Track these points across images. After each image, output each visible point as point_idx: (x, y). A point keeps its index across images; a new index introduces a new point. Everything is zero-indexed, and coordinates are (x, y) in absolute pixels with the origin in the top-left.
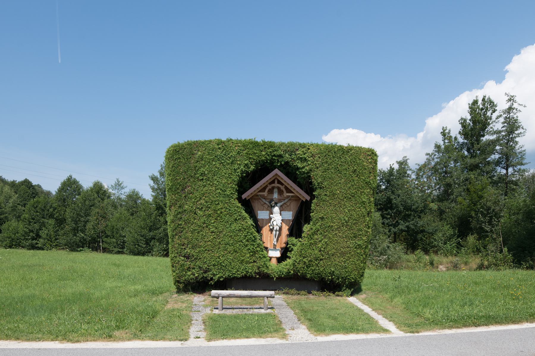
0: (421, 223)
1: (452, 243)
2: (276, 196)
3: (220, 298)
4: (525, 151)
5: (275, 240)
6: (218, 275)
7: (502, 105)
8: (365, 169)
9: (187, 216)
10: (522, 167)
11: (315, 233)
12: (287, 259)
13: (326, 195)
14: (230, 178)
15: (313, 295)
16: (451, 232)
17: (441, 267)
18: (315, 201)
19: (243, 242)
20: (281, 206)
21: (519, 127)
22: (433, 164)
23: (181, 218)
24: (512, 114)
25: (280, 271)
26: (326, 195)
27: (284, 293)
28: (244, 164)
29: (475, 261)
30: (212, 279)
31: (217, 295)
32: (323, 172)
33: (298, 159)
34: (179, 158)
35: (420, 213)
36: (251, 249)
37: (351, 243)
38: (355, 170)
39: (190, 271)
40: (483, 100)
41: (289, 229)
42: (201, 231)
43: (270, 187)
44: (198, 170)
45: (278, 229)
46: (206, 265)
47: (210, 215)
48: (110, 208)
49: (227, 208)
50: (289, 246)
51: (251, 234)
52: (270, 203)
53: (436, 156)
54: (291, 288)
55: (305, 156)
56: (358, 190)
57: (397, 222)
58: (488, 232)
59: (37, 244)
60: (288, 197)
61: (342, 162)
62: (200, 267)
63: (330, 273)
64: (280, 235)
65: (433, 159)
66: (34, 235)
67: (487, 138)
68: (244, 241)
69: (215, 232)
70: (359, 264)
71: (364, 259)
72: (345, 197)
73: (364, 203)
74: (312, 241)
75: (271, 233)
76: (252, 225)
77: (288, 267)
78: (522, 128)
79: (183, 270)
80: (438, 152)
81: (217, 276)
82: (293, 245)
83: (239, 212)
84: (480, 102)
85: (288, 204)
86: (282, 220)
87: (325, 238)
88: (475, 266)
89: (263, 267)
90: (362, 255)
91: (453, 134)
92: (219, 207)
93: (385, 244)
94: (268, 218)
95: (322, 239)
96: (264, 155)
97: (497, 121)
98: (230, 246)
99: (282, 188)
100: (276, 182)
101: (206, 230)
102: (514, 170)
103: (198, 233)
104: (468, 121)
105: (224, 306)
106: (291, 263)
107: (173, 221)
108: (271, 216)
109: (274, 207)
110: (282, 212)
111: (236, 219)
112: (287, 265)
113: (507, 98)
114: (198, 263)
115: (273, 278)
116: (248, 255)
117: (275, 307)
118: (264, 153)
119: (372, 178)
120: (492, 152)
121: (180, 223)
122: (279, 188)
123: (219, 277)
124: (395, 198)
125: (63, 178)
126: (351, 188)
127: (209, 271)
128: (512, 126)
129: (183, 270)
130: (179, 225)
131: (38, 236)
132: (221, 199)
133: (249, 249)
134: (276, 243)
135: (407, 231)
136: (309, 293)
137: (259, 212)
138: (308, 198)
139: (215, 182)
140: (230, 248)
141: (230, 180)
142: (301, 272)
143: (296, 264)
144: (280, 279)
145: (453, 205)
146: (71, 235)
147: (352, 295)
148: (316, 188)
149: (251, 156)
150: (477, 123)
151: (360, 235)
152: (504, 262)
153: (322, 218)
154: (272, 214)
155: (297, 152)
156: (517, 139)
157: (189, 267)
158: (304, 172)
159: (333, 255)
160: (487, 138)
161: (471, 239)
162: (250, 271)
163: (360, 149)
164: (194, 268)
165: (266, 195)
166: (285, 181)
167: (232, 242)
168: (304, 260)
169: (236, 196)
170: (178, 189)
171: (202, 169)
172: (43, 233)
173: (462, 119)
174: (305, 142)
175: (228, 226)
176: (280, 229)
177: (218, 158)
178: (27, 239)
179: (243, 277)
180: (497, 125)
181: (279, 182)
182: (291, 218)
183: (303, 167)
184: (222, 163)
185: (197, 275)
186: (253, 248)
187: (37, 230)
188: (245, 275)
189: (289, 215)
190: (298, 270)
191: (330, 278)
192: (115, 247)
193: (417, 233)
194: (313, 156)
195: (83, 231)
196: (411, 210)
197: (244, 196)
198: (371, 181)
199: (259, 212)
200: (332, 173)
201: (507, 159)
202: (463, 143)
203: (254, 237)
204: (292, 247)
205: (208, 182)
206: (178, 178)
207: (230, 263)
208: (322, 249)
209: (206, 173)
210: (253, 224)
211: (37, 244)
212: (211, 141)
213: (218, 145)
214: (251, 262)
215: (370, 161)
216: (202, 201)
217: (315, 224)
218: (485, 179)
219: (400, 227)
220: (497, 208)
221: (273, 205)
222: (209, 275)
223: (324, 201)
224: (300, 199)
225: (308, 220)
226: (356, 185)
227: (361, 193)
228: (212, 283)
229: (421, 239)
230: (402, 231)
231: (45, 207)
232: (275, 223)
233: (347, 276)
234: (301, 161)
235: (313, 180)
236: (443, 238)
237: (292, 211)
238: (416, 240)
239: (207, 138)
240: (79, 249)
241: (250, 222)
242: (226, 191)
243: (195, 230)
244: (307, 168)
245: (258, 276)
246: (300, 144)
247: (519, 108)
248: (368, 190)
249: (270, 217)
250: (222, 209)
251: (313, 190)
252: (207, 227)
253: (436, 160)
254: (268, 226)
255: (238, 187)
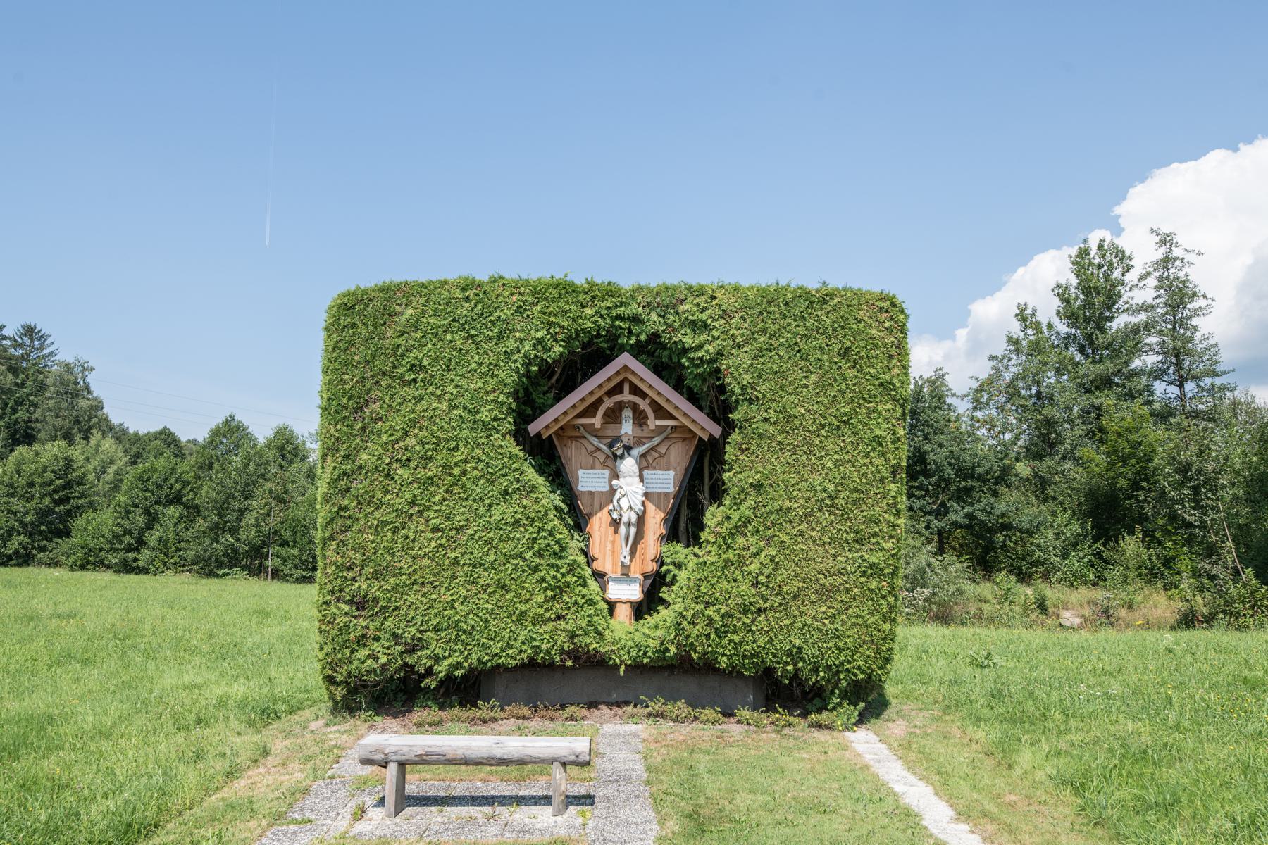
0: (1001, 507)
1: (1081, 554)
2: (627, 428)
3: (393, 767)
4: (1216, 345)
5: (626, 551)
6: (444, 658)
7: (1144, 253)
8: (876, 346)
9: (366, 483)
10: (1218, 381)
11: (738, 530)
12: (660, 608)
13: (765, 420)
14: (493, 376)
15: (739, 722)
16: (1076, 527)
17: (1065, 614)
18: (735, 437)
19: (524, 560)
20: (643, 456)
21: (1195, 294)
22: (1007, 377)
23: (348, 490)
24: (1172, 270)
25: (639, 646)
26: (765, 420)
27: (650, 715)
28: (533, 340)
29: (1159, 604)
30: (429, 672)
31: (380, 757)
32: (755, 358)
33: (683, 325)
34: (354, 325)
35: (996, 484)
36: (548, 578)
37: (849, 560)
38: (848, 348)
39: (364, 645)
40: (1100, 247)
41: (665, 521)
42: (404, 526)
43: (608, 403)
44: (402, 355)
45: (634, 520)
46: (413, 630)
47: (430, 481)
48: (302, 481)
49: (480, 461)
50: (665, 568)
51: (551, 534)
52: (611, 446)
53: (1013, 362)
54: (672, 698)
55: (704, 316)
56: (860, 406)
57: (943, 504)
58: (1195, 527)
59: (135, 560)
60: (661, 429)
61: (807, 329)
62: (395, 636)
63: (789, 654)
64: (639, 536)
65: (1007, 368)
66: (133, 541)
67: (1120, 322)
68: (527, 555)
69: (442, 530)
70: (876, 623)
71: (891, 608)
72: (823, 426)
73: (878, 440)
74: (730, 555)
75: (616, 532)
76: (556, 508)
77: (660, 633)
78: (1204, 296)
79: (345, 644)
80: (1017, 352)
81: (446, 663)
82: (679, 566)
83: (516, 470)
84: (1094, 251)
85: (662, 449)
86: (646, 495)
87: (768, 544)
88: (1172, 618)
89: (586, 634)
90: (884, 597)
91: (1043, 318)
92: (458, 456)
93: (923, 558)
94: (607, 488)
95: (762, 550)
96: (590, 318)
97: (1141, 285)
98: (486, 570)
99: (644, 405)
100: (626, 388)
101: (417, 524)
102: (1198, 386)
103: (394, 533)
104: (1073, 290)
105: (410, 789)
106: (669, 620)
107: (326, 500)
108: (614, 482)
109: (622, 457)
110: (645, 472)
111: (506, 493)
112: (657, 627)
113: (1157, 239)
114: (389, 623)
115: (616, 667)
116: (540, 598)
117: (599, 794)
118: (589, 311)
119: (896, 371)
120: (1135, 351)
121: (345, 502)
122: (635, 407)
123: (450, 666)
124: (933, 450)
125: (217, 420)
126: (840, 398)
127: (422, 649)
128: (1179, 296)
129: (345, 644)
130: (341, 509)
131: (141, 543)
132: (465, 433)
133: (543, 579)
134: (627, 561)
135: (969, 527)
136: (728, 714)
137: (581, 472)
138: (716, 431)
139: (450, 389)
140: (485, 578)
141: (493, 382)
142: (700, 649)
143: (685, 624)
144: (637, 668)
145: (1067, 466)
146: (207, 541)
147: (862, 720)
148: (737, 401)
149: (553, 319)
150: (1092, 298)
151: (875, 535)
152: (1252, 607)
153: (758, 487)
154: (617, 477)
155: (682, 308)
156: (1194, 322)
157: (364, 636)
158: (701, 359)
159: (795, 597)
160: (1120, 322)
161: (1130, 545)
162: (544, 647)
163: (858, 294)
164: (377, 639)
165: (598, 426)
166: (650, 386)
167: (491, 558)
168: (709, 612)
169: (508, 425)
170: (345, 407)
171: (415, 353)
172: (152, 538)
173: (1058, 286)
174: (703, 283)
175: (482, 511)
176: (641, 519)
177: (462, 324)
178: (116, 550)
179: (523, 665)
180: (1140, 293)
181: (635, 390)
182: (671, 489)
183: (700, 347)
184: (472, 336)
185: (383, 659)
186: (554, 577)
187: (141, 529)
188: (531, 660)
189: (666, 481)
190: (692, 644)
191: (790, 667)
192: (296, 567)
193: (992, 531)
194: (725, 315)
195: (234, 532)
196: (972, 477)
197: (533, 428)
198: (895, 381)
199: (581, 472)
200: (781, 357)
201: (1179, 364)
202: (1068, 336)
203: (557, 542)
204: (676, 572)
205: (430, 389)
206: (346, 377)
207: (486, 621)
208: (762, 579)
209: (425, 362)
210: (563, 506)
211: (135, 560)
212: (443, 283)
213: (464, 290)
214: (550, 620)
215: (887, 324)
216: (410, 441)
217: (736, 505)
218: (1136, 406)
219: (952, 516)
220: (1210, 467)
221: (619, 453)
222: (421, 660)
223: (761, 436)
224: (695, 435)
225: (717, 494)
226: (852, 391)
227: (868, 414)
228: (431, 683)
229: (1004, 546)
230: (956, 525)
231: (165, 480)
232: (624, 503)
233: (842, 663)
234: (694, 330)
235: (727, 380)
236: (1058, 544)
237: (675, 469)
238: (990, 547)
239: (436, 276)
240: (220, 572)
241: (550, 499)
242: (478, 412)
243: (384, 523)
244: (711, 348)
245: (569, 663)
246: (690, 288)
247: (1188, 257)
248: (889, 406)
249: (611, 486)
250: (465, 461)
251: (727, 408)
252: (420, 513)
253: (1014, 369)
254: (605, 510)
255: (517, 399)
